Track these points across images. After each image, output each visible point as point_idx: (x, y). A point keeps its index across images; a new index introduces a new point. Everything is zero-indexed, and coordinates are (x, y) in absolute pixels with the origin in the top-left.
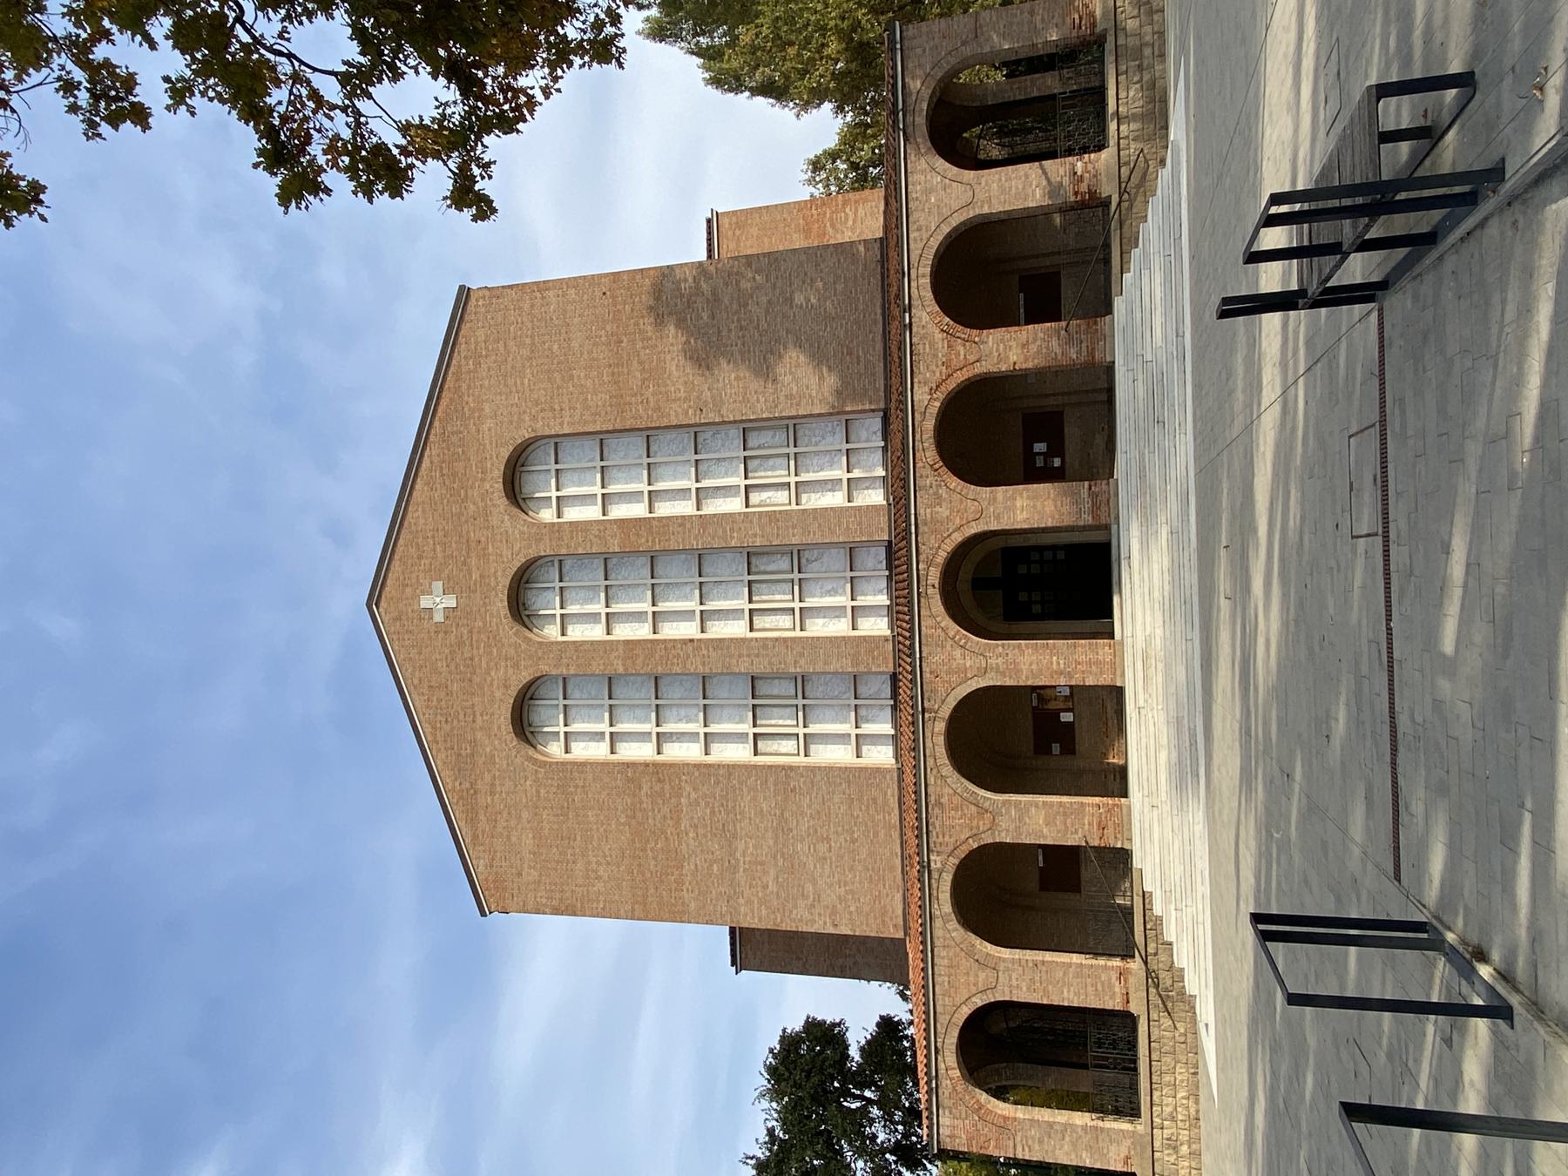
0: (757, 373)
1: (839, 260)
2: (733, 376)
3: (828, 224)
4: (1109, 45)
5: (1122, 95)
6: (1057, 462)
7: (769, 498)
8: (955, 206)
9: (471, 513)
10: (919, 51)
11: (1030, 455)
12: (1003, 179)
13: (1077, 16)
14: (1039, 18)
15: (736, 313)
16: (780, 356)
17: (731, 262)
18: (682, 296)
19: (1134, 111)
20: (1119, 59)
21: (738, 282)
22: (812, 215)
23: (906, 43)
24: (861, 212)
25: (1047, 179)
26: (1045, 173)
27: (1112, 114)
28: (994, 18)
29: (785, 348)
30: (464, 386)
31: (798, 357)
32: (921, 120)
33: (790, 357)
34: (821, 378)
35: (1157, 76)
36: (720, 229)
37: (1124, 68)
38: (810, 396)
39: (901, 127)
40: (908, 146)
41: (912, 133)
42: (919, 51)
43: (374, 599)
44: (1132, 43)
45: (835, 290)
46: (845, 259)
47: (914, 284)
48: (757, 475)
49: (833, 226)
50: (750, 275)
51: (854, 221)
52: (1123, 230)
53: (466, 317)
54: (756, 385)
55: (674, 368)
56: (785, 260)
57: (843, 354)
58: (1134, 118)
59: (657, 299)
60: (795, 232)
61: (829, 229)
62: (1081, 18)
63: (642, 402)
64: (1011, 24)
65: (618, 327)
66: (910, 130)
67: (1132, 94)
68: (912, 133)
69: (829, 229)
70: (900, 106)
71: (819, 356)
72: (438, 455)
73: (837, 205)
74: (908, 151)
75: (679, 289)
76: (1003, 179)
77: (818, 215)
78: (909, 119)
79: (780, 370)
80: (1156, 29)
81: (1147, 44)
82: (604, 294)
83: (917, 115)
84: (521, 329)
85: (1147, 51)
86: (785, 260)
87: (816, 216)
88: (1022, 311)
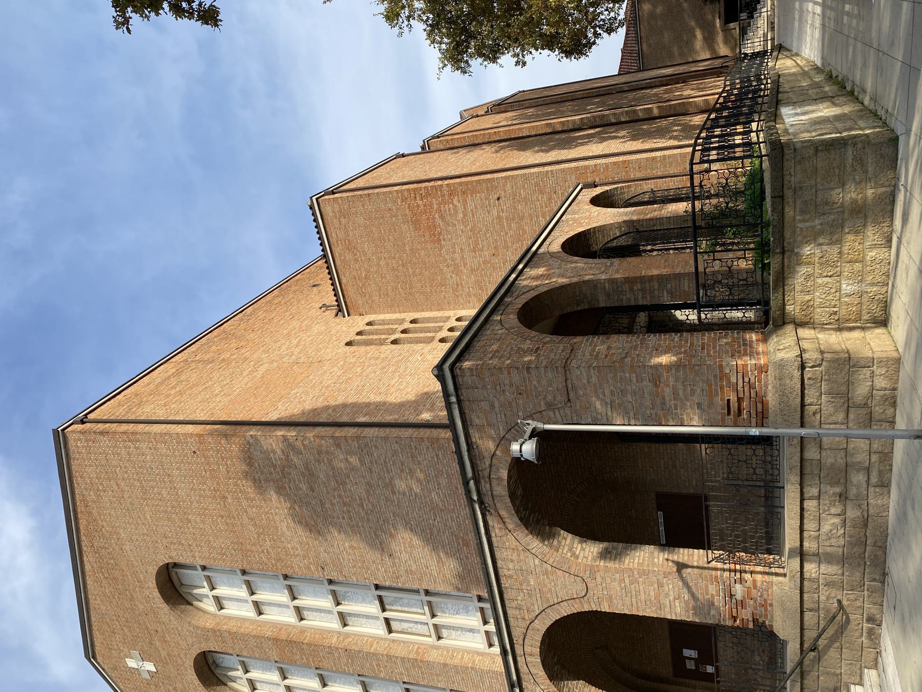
0: (372, 546)
1: (437, 455)
2: (347, 545)
3: (437, 216)
4: (789, 458)
5: (810, 525)
6: (710, 669)
7: (410, 627)
8: (563, 595)
9: (141, 610)
10: (485, 405)
11: (679, 660)
12: (627, 581)
13: (733, 398)
14: (668, 391)
15: (335, 490)
16: (392, 536)
17: (318, 440)
18: (275, 466)
19: (829, 550)
20: (806, 477)
21: (330, 461)
22: (418, 206)
23: (464, 393)
24: (470, 205)
25: (693, 595)
26: (686, 584)
27: (791, 551)
28: (594, 379)
29: (395, 528)
30: (95, 512)
31: (411, 539)
32: (501, 490)
33: (403, 538)
34: (440, 561)
35: (871, 511)
36: (325, 217)
37: (814, 491)
38: (431, 575)
39: (475, 498)
40: (489, 518)
41: (491, 503)
42: (485, 405)
43: (90, 653)
44: (830, 460)
45: (439, 484)
46: (444, 455)
47: (520, 660)
48: (393, 608)
49: (442, 217)
50: (341, 457)
51: (465, 215)
52: (805, 682)
53: (72, 455)
54: (372, 556)
55: (285, 529)
56: (376, 447)
57: (459, 544)
58: (829, 558)
59: (250, 465)
60: (404, 223)
61: (439, 221)
62: (740, 400)
63: (263, 552)
64: (623, 392)
65: (218, 484)
66: (488, 500)
67: (826, 528)
68: (491, 503)
69: (439, 221)
70: (472, 483)
71: (432, 539)
72: (96, 562)
73: (443, 196)
74: (491, 523)
75: (270, 459)
76: (627, 581)
77: (424, 205)
78: (485, 487)
79: (393, 546)
80: (875, 446)
81: (859, 468)
82: (195, 452)
83: (494, 483)
84: (126, 473)
85: (858, 478)
86: (376, 447)
87: (422, 207)
88: (662, 528)
